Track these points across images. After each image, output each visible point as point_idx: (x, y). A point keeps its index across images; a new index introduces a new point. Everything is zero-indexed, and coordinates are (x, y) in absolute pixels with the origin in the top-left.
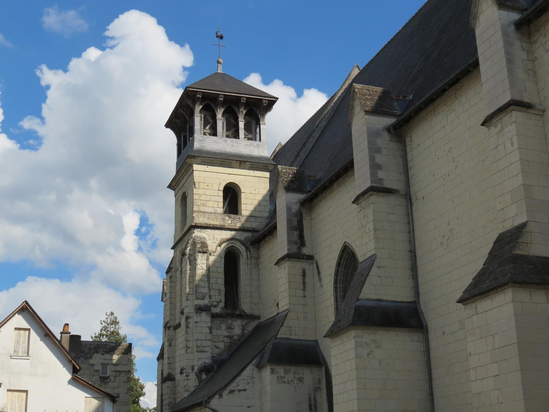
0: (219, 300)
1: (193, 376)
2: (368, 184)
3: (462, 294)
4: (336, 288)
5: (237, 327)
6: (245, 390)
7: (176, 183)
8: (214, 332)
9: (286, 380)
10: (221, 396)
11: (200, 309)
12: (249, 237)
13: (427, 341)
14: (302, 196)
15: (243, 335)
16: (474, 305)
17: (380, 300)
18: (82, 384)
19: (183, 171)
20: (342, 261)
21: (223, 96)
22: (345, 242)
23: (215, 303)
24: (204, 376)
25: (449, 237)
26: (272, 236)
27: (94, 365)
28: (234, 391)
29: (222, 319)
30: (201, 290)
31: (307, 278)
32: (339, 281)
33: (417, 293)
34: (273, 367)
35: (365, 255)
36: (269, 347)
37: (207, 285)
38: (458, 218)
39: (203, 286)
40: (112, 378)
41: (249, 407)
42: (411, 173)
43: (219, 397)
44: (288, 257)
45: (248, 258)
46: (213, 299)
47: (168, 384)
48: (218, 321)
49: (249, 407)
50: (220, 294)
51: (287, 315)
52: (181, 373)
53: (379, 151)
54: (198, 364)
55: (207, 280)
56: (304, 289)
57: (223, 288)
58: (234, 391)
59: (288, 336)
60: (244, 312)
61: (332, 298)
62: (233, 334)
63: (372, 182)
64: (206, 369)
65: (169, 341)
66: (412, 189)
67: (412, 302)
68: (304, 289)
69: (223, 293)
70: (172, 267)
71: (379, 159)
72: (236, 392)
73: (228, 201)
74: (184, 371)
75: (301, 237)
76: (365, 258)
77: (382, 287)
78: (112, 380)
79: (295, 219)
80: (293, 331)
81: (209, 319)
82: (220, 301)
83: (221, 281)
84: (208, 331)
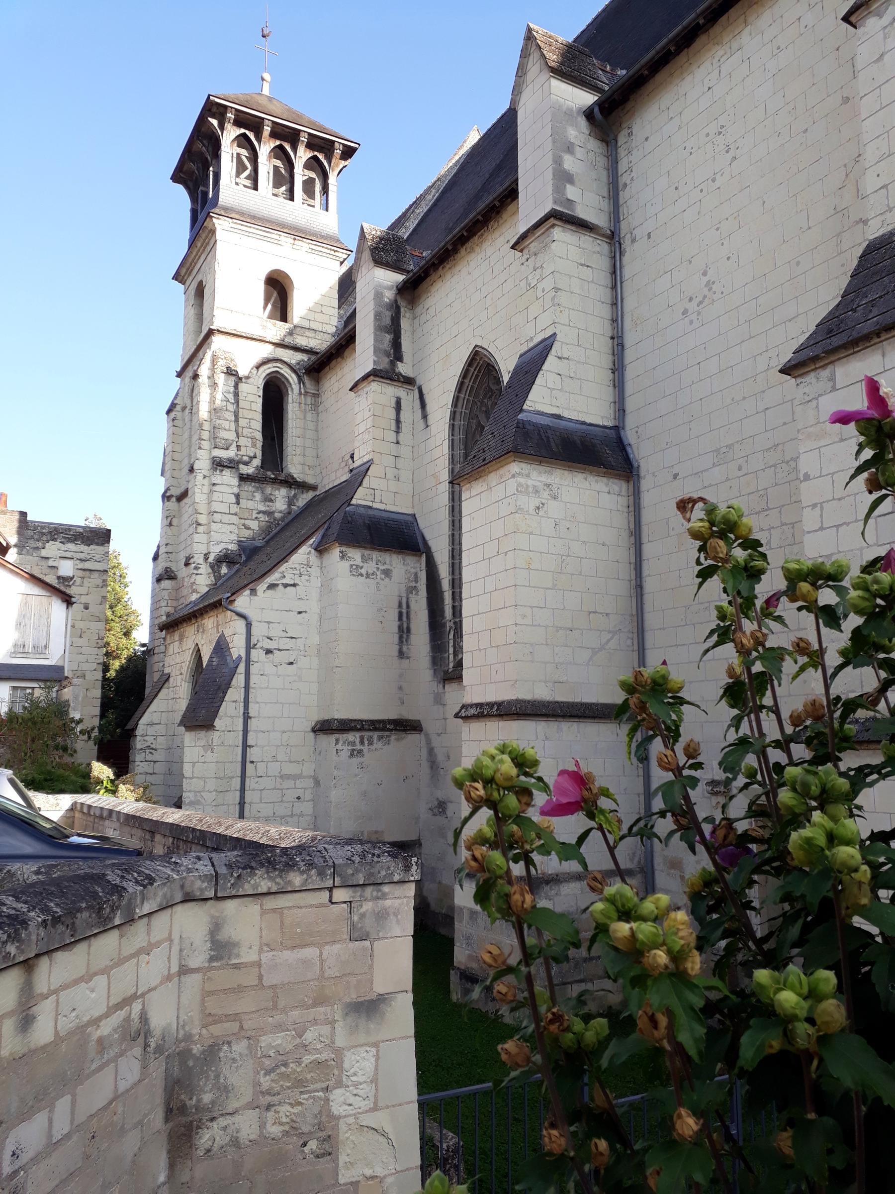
0: (252, 455)
1: (205, 569)
2: (369, 367)
3: (790, 355)
4: (452, 427)
5: (280, 499)
6: (294, 585)
7: (188, 269)
8: (243, 502)
9: (363, 571)
10: (253, 592)
11: (219, 465)
12: (303, 360)
13: (636, 494)
14: (399, 278)
15: (289, 513)
16: (825, 373)
17: (558, 417)
18: (12, 571)
19: (199, 245)
20: (467, 381)
21: (270, 123)
22: (476, 346)
23: (246, 459)
24: (224, 570)
25: (705, 297)
26: (343, 358)
27: (48, 558)
28: (277, 585)
29: (257, 485)
30: (223, 434)
31: (402, 413)
32: (458, 416)
33: (621, 410)
34: (344, 549)
35: (532, 339)
36: (338, 517)
37: (233, 427)
38: (728, 258)
39: (227, 428)
40: (78, 581)
41: (300, 613)
42: (623, 196)
43: (251, 594)
44: (375, 374)
45: (300, 394)
46: (243, 452)
47: (166, 584)
48: (249, 487)
49: (300, 613)
50: (254, 445)
51: (368, 469)
52: (187, 564)
53: (570, 149)
54: (216, 550)
55: (233, 418)
56: (398, 431)
57: (259, 436)
58: (277, 585)
59: (370, 504)
60: (292, 477)
61: (446, 444)
62: (274, 509)
63: (555, 202)
64: (227, 558)
65: (169, 519)
66: (624, 225)
67: (611, 428)
68: (398, 431)
69: (260, 444)
70: (176, 404)
71: (569, 163)
72: (281, 587)
73: (272, 301)
74: (192, 561)
75: (396, 344)
76: (531, 345)
77: (566, 395)
78: (77, 584)
79: (388, 314)
80: (379, 495)
81: (235, 481)
82: (255, 457)
83: (258, 425)
84: (234, 500)
